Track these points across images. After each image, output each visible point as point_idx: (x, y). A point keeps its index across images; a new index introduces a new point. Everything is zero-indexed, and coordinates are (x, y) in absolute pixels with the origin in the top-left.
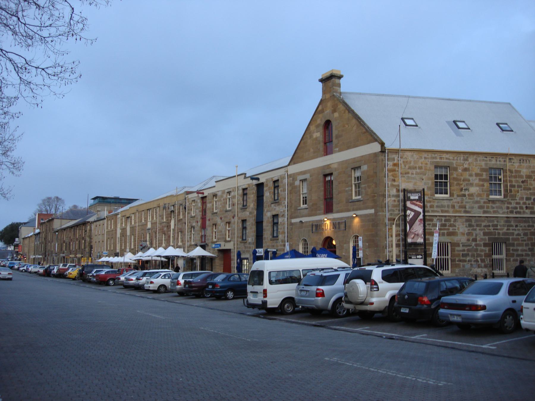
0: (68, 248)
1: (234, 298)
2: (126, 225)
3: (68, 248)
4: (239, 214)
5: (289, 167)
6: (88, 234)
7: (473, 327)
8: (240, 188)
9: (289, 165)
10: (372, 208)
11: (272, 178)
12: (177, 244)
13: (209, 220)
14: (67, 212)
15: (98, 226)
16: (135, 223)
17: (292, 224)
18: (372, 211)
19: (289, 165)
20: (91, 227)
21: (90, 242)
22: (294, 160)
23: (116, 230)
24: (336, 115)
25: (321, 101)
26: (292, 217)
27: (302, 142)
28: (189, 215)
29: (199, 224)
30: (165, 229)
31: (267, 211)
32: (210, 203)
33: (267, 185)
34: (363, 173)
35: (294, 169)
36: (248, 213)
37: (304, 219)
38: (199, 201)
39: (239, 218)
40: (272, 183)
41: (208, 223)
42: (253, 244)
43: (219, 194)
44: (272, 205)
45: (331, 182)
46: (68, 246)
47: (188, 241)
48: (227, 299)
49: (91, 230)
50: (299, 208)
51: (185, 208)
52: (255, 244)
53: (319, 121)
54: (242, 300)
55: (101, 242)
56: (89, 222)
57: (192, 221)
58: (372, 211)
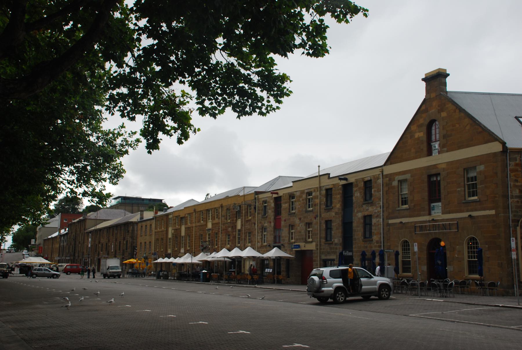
4: (323, 215)
8: (324, 189)
11: (363, 179)
13: (285, 220)
17: (388, 225)
18: (493, 212)
24: (444, 114)
26: (389, 218)
30: (230, 229)
33: (357, 186)
35: (389, 170)
36: (333, 214)
37: (404, 220)
38: (272, 201)
51: (255, 208)
53: (421, 121)
57: (263, 222)
58: (493, 212)
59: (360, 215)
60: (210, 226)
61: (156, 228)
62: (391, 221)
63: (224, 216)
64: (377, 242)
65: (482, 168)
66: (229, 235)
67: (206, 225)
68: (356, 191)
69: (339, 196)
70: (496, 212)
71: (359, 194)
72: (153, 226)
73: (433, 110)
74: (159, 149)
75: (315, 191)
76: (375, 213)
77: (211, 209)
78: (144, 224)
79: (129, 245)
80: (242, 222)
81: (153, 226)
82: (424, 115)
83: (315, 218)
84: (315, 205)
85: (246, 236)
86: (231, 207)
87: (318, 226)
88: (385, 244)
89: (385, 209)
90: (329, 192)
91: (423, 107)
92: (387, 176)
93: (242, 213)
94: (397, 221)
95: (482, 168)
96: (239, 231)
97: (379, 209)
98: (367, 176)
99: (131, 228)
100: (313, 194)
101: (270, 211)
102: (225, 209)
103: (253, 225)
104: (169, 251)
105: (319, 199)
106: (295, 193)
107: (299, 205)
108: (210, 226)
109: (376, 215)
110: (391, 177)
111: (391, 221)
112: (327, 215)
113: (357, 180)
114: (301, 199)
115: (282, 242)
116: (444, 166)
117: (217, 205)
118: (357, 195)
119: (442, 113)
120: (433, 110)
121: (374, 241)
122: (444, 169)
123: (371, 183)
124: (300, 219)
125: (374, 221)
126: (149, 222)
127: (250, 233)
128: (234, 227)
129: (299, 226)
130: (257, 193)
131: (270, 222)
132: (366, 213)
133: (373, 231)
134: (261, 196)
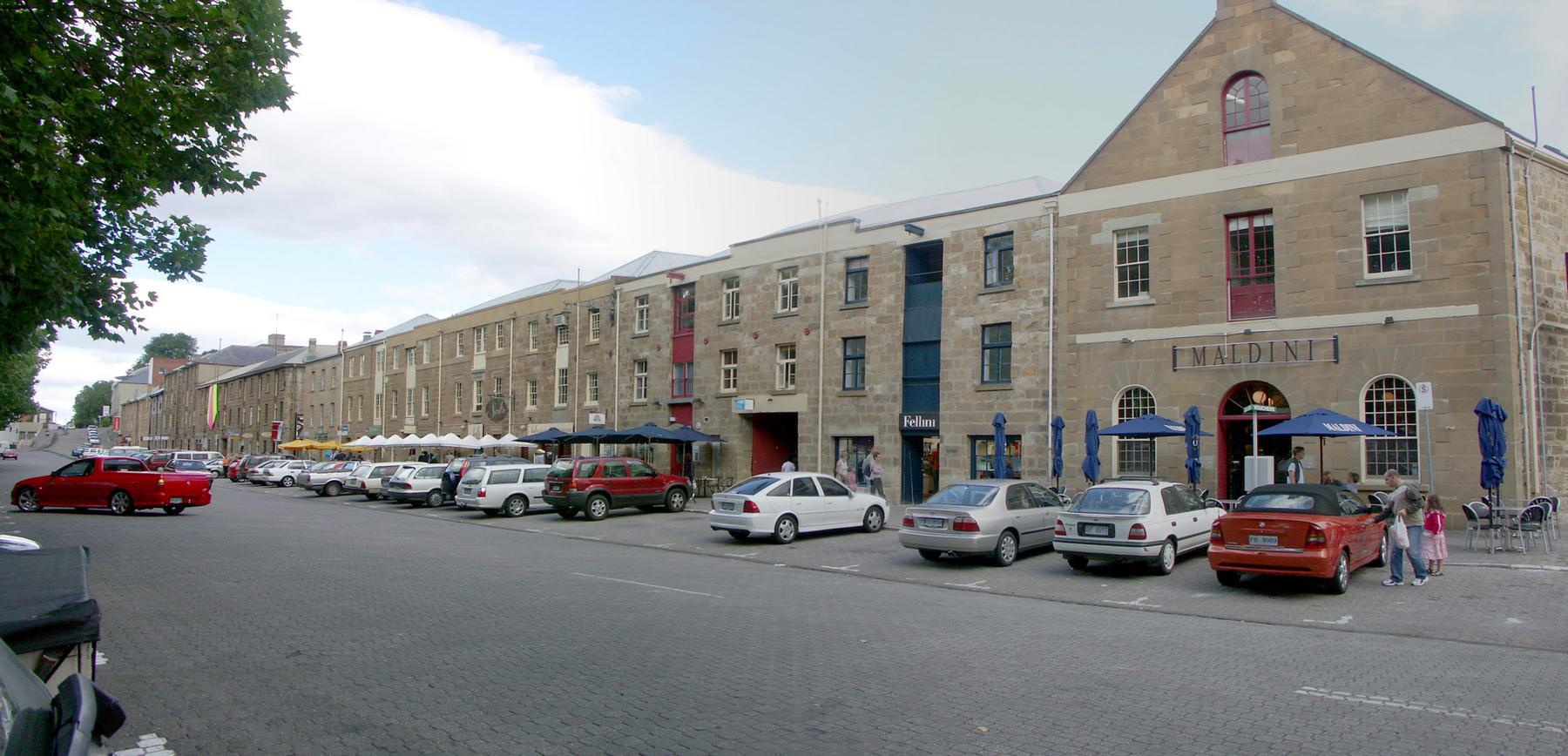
0: (234, 420)
1: (607, 516)
2: (403, 365)
3: (234, 420)
4: (833, 325)
5: (1061, 198)
6: (288, 391)
7: (1091, 562)
8: (837, 257)
9: (1063, 192)
10: (1469, 300)
11: (980, 230)
12: (580, 405)
13: (706, 342)
14: (225, 351)
15: (319, 373)
16: (433, 358)
17: (1074, 347)
18: (1473, 310)
19: (1063, 192)
20: (295, 377)
21: (293, 407)
22: (1083, 179)
23: (372, 379)
24: (1282, 57)
25: (1215, 22)
26: (1076, 329)
27: (1125, 129)
28: (628, 333)
29: (667, 352)
30: (537, 369)
31: (959, 315)
32: (710, 298)
33: (958, 247)
34: (1416, 207)
35: (1072, 205)
36: (873, 321)
37: (1134, 335)
38: (664, 297)
39: (832, 334)
40: (981, 241)
41: (699, 348)
42: (895, 398)
43: (746, 275)
44: (983, 299)
45: (1269, 231)
46: (235, 415)
47: (621, 396)
48: (589, 518)
49: (295, 382)
50: (1109, 305)
51: (613, 317)
52: (900, 399)
53: (1202, 76)
54: (801, 530)
55: (327, 405)
56: (291, 366)
57: (636, 348)
58: (1473, 310)
59: (969, 323)
60: (480, 363)
61: (346, 373)
62: (1081, 339)
63: (520, 340)
64: (1029, 394)
65: (1430, 192)
66: (534, 383)
67: (471, 362)
68: (956, 260)
69: (893, 275)
70: (1481, 309)
71: (964, 270)
72: (341, 369)
73: (1246, 48)
74: (795, 414)
75: (806, 264)
76: (1024, 317)
77: (485, 326)
78: (318, 366)
79: (287, 410)
80: (572, 351)
81: (341, 369)
82: (1212, 61)
83: (807, 332)
84: (808, 300)
85: (583, 384)
86: (542, 318)
87: (821, 354)
88: (1060, 399)
89: (1062, 303)
90: (857, 273)
91: (1209, 41)
92: (1071, 220)
93: (574, 330)
94: (1117, 336)
95: (1430, 192)
96: (564, 372)
97: (1040, 307)
98: (996, 222)
99: (290, 377)
100: (802, 272)
101: (657, 321)
102: (523, 323)
103: (606, 356)
104: (377, 422)
105: (827, 286)
106: (739, 273)
107: (754, 300)
108: (480, 363)
109: (1028, 322)
110: (1088, 223)
111: (1081, 339)
112: (852, 325)
113: (957, 235)
114: (759, 287)
115: (697, 395)
116: (1288, 190)
117: (502, 316)
118: (957, 272)
119: (1277, 55)
120: (1246, 48)
121: (1018, 391)
122: (1285, 199)
123: (1011, 240)
124: (756, 336)
125: (1017, 338)
126: (329, 363)
127: (595, 376)
128: (548, 363)
129: (751, 353)
130: (619, 280)
131: (659, 348)
132: (991, 319)
133: (1013, 364)
134: (627, 287)
